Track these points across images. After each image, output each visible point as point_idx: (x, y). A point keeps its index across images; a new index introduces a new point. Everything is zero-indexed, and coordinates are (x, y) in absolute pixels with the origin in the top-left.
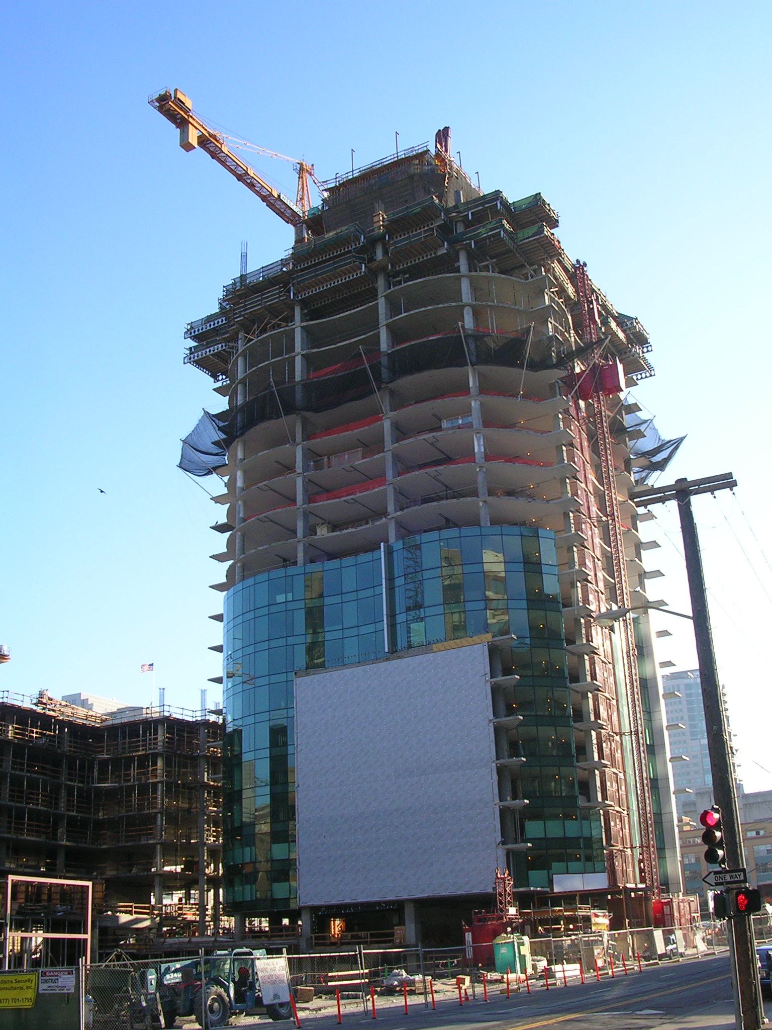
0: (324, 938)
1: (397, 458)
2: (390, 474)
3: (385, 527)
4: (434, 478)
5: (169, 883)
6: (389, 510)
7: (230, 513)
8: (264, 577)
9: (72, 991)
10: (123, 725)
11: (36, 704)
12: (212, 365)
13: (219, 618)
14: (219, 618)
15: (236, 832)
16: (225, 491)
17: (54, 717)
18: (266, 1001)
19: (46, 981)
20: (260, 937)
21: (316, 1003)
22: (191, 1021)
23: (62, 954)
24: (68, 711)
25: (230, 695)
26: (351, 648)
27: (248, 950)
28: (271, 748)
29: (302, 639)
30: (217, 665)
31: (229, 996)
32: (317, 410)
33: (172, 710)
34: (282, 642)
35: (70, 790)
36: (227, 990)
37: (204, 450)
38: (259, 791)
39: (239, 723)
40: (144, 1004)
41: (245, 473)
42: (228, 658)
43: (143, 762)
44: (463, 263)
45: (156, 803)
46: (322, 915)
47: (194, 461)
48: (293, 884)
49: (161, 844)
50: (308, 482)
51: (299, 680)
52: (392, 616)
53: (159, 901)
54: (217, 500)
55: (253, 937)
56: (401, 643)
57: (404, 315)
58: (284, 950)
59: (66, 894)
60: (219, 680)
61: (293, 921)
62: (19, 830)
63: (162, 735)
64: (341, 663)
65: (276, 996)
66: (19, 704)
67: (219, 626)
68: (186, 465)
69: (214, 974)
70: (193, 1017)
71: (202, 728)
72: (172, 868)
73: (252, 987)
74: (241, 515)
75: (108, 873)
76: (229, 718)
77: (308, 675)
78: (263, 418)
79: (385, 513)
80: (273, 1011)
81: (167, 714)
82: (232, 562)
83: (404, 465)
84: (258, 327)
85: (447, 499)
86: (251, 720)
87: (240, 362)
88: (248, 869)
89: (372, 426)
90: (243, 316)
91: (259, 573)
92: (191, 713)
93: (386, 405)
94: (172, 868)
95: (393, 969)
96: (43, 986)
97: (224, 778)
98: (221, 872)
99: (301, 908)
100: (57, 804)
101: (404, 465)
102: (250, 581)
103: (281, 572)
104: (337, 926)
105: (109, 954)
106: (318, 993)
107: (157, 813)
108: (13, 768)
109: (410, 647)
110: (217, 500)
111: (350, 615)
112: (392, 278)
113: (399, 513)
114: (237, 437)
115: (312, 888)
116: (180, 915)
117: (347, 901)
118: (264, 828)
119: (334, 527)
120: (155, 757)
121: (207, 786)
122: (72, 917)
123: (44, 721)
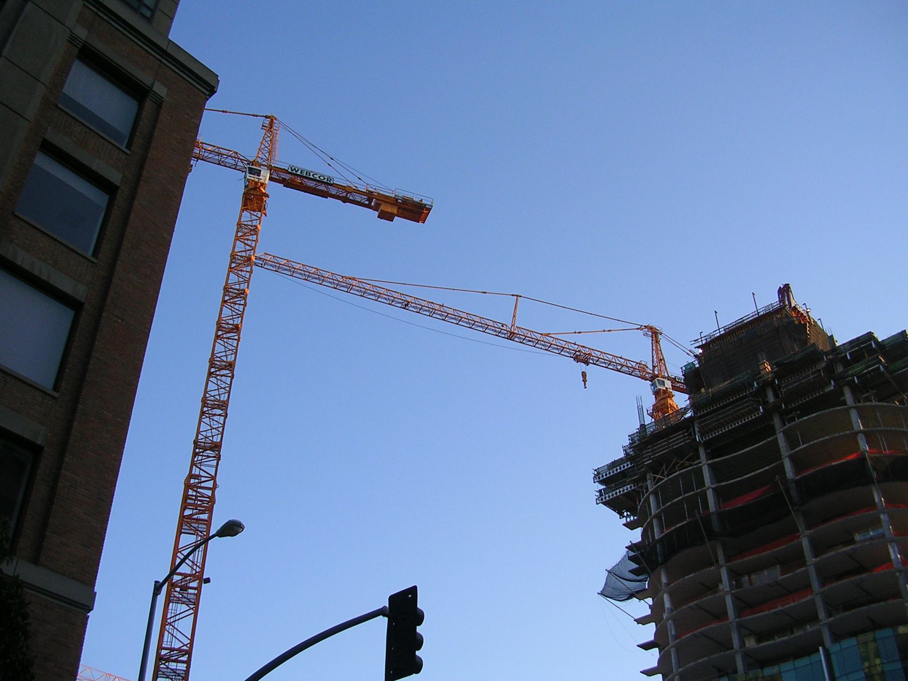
6: (820, 617)
41: (671, 595)
44: (848, 396)
57: (802, 447)
84: (666, 469)
87: (652, 499)
93: (801, 524)
112: (786, 417)
119: (760, 638)
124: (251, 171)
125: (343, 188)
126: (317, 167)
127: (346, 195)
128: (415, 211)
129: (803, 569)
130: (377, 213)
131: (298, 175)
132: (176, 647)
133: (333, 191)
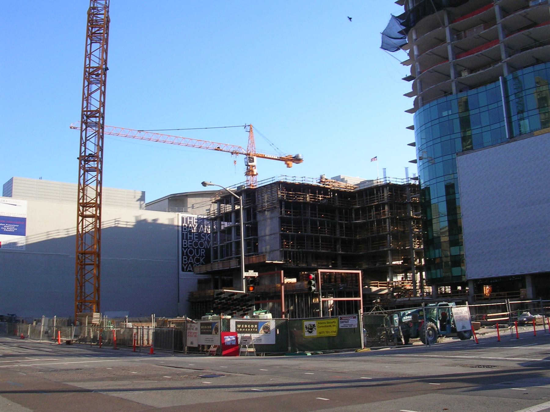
0: (481, 296)
1: (504, 27)
2: (501, 37)
3: (501, 68)
4: (528, 36)
5: (396, 270)
7: (412, 70)
8: (435, 102)
9: (356, 326)
10: (366, 190)
11: (319, 183)
13: (412, 128)
14: (412, 128)
15: (431, 242)
16: (408, 58)
17: (329, 188)
18: (459, 329)
19: (342, 322)
20: (446, 296)
21: (481, 330)
22: (417, 341)
23: (352, 308)
24: (336, 185)
25: (421, 169)
26: (487, 138)
27: (446, 303)
28: (446, 195)
29: (474, 132)
30: (413, 153)
31: (437, 327)
32: (455, 6)
33: (391, 179)
34: (448, 137)
35: (341, 225)
36: (436, 324)
37: (394, 37)
38: (441, 219)
39: (428, 183)
40: (393, 332)
41: (418, 47)
42: (419, 150)
43: (377, 208)
45: (386, 229)
46: (479, 284)
47: (389, 44)
48: (463, 268)
49: (390, 250)
50: (454, 47)
51: (459, 158)
52: (509, 117)
53: (392, 280)
54: (405, 63)
55: (443, 297)
56: (516, 132)
58: (467, 302)
59: (344, 278)
60: (414, 162)
61: (463, 288)
62: (317, 248)
63: (386, 194)
64: (482, 146)
65: (463, 327)
66: (311, 183)
67: (412, 132)
68: (385, 47)
69: (428, 316)
70: (418, 339)
71: (407, 189)
72: (397, 262)
73: (449, 322)
74: (419, 70)
75: (364, 266)
76: (422, 182)
77: (463, 154)
78: (425, 14)
79: (499, 60)
80: (460, 335)
81: (388, 182)
82: (416, 97)
83: (509, 31)
85: (536, 47)
86: (434, 181)
88: (437, 261)
89: (488, 10)
91: (432, 100)
92: (401, 181)
94: (397, 262)
95: (523, 312)
96: (341, 325)
97: (421, 213)
98: (423, 263)
99: (468, 281)
100: (335, 233)
101: (509, 31)
102: (427, 106)
103: (444, 99)
104: (487, 290)
105: (373, 307)
106: (482, 325)
107: (387, 234)
108: (311, 216)
109: (521, 134)
110: (405, 63)
111: (485, 119)
113: (509, 59)
114: (412, 27)
115: (473, 270)
116: (403, 286)
117: (493, 276)
118: (445, 239)
119: (471, 71)
120: (383, 205)
121: (412, 218)
122: (347, 290)
123: (324, 191)
129: (495, 26)
132: (91, 209)
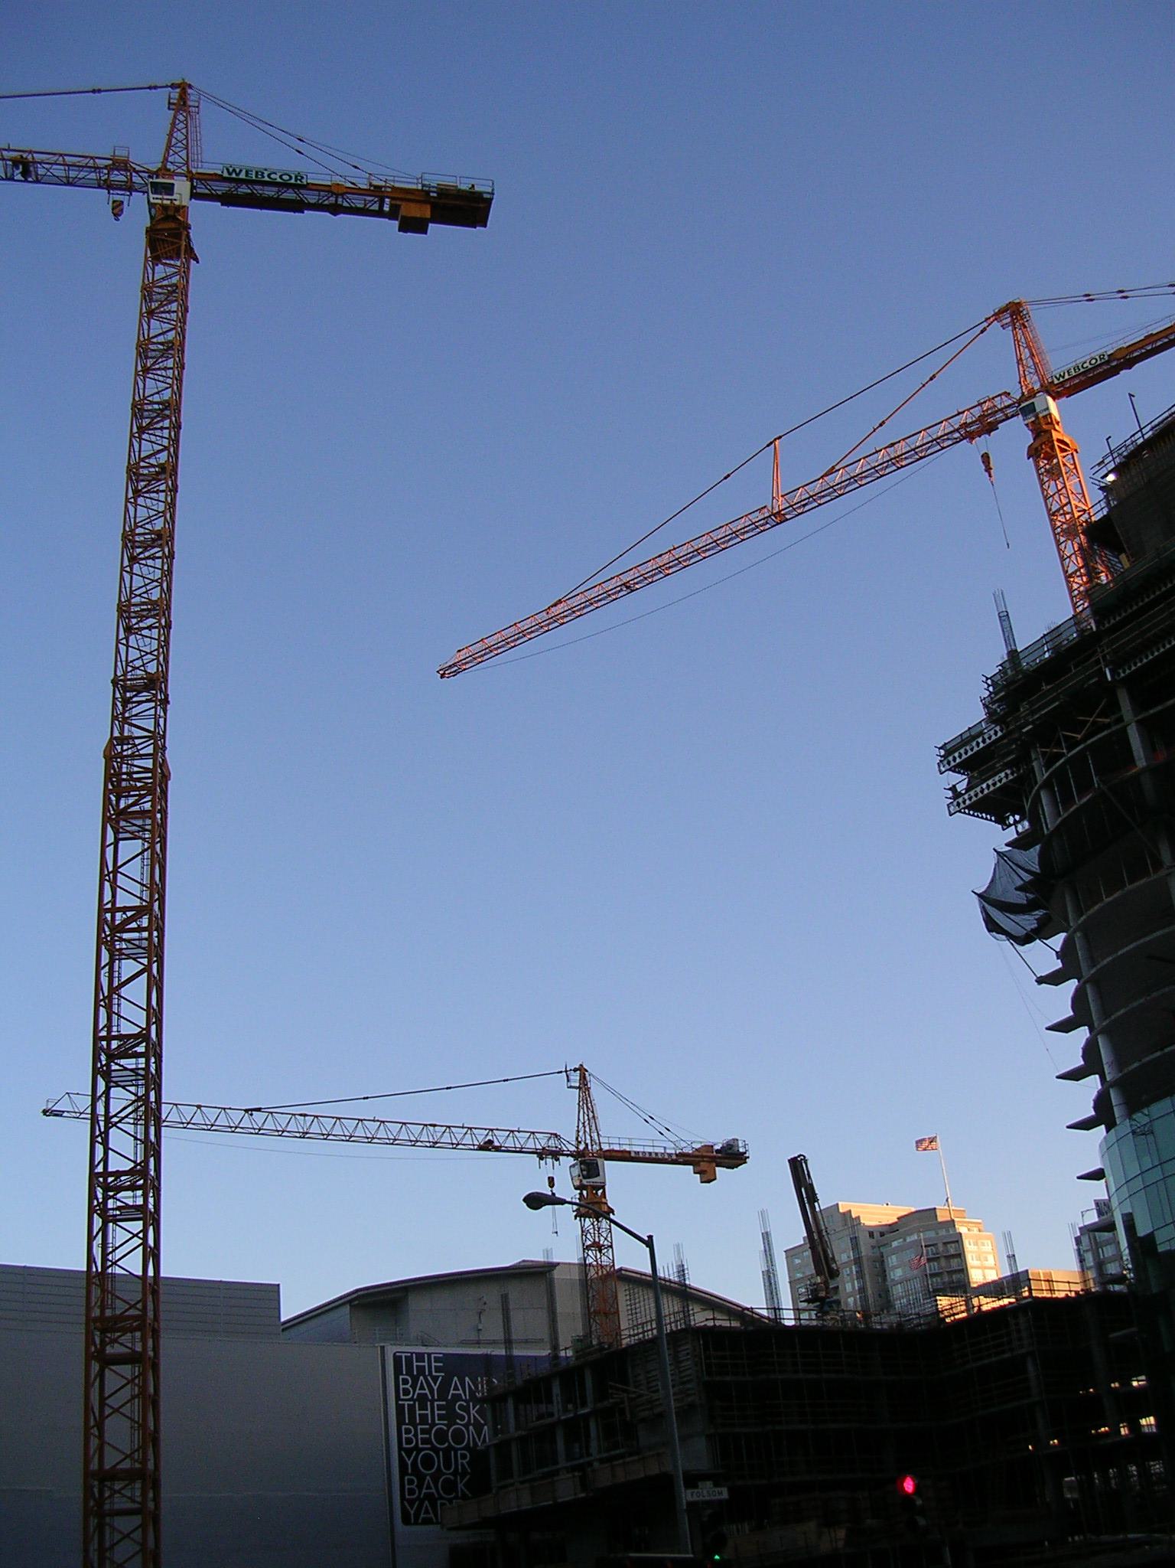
12: (994, 807)
16: (1059, 965)
87: (1044, 797)
90: (1032, 723)
92: (1066, 1287)
124: (157, 188)
125: (328, 189)
126: (273, 159)
127: (335, 201)
128: (466, 208)
130: (396, 223)
131: (242, 181)
133: (312, 199)
